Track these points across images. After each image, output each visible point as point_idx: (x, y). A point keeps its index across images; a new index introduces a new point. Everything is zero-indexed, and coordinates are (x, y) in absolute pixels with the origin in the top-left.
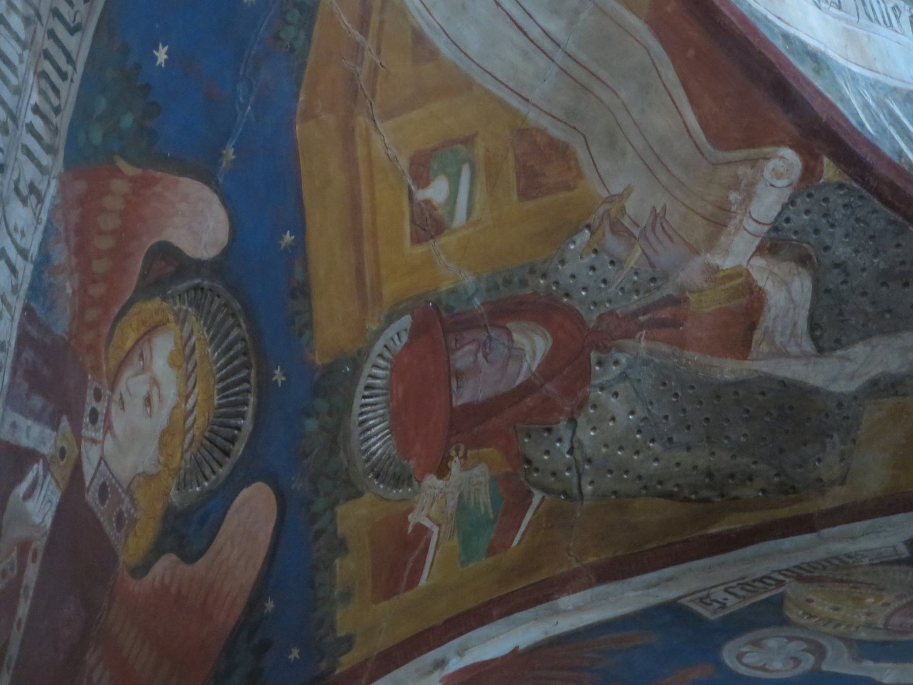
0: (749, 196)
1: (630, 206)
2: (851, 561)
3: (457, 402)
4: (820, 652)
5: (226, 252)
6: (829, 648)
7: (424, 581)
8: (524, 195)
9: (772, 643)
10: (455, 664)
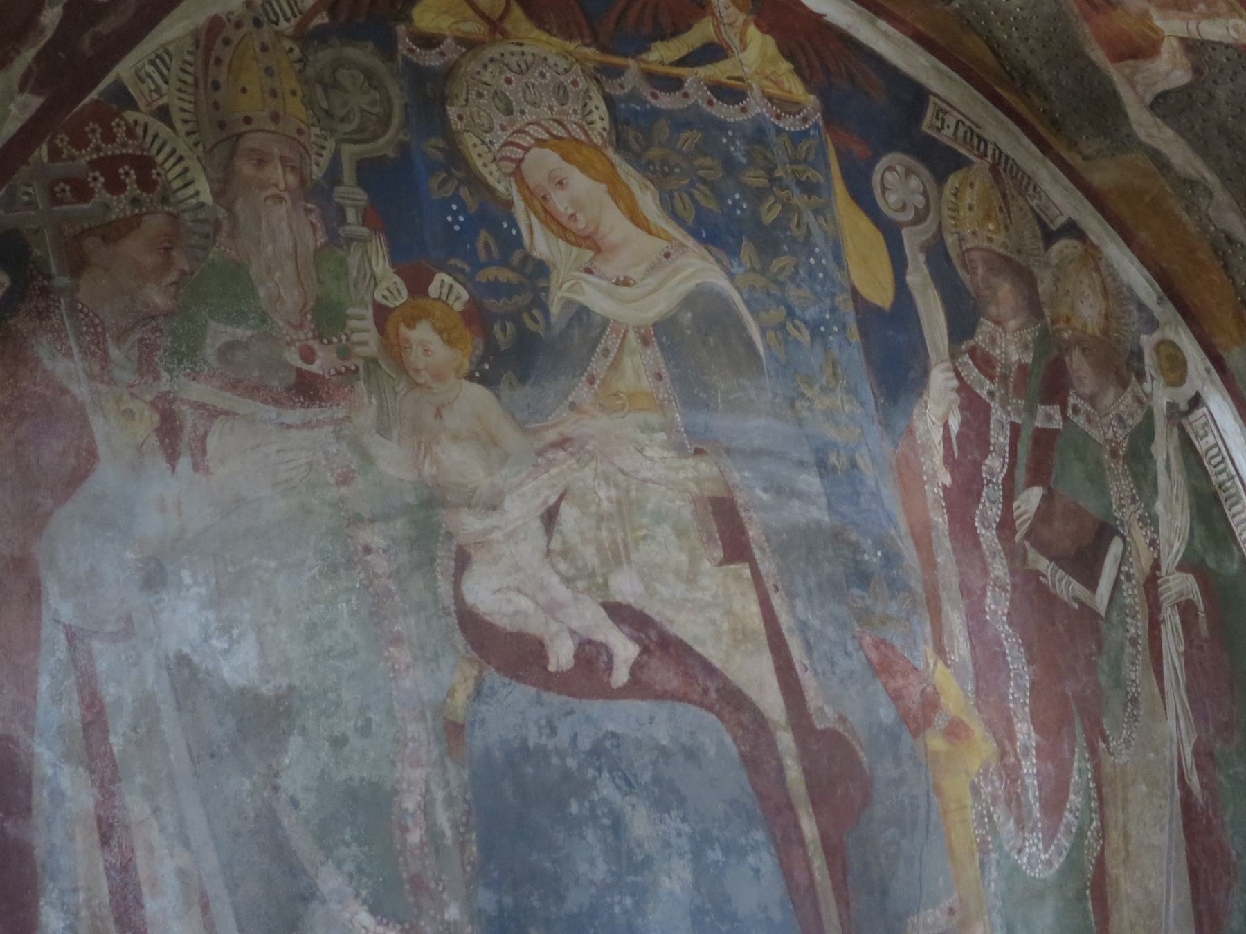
2: (1031, 190)
6: (927, 223)
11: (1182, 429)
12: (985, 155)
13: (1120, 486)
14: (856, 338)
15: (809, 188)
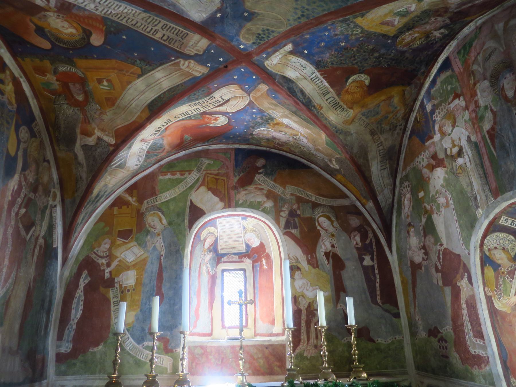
0: (107, 135)
1: (105, 116)
3: (70, 84)
4: (25, 142)
5: (92, 45)
7: (37, 75)
8: (106, 98)
9: (27, 135)
10: (21, 80)
11: (51, 210)
12: (40, 138)
13: (39, 216)
14: (4, 159)
15: (8, 122)
